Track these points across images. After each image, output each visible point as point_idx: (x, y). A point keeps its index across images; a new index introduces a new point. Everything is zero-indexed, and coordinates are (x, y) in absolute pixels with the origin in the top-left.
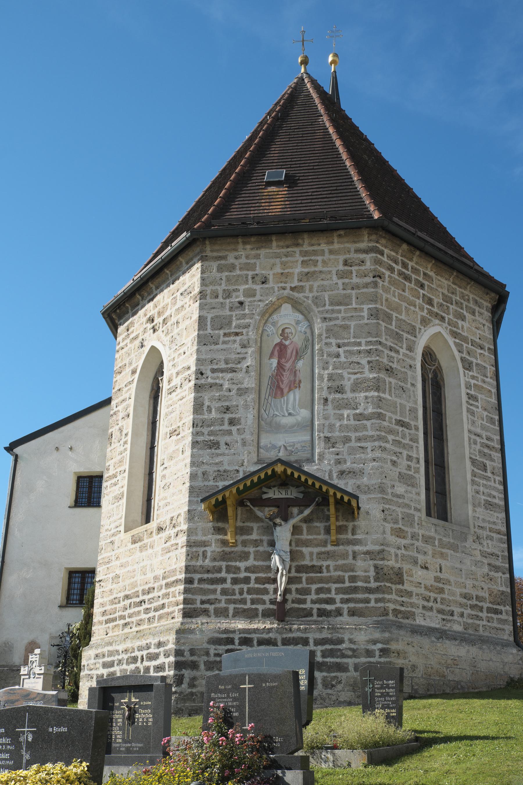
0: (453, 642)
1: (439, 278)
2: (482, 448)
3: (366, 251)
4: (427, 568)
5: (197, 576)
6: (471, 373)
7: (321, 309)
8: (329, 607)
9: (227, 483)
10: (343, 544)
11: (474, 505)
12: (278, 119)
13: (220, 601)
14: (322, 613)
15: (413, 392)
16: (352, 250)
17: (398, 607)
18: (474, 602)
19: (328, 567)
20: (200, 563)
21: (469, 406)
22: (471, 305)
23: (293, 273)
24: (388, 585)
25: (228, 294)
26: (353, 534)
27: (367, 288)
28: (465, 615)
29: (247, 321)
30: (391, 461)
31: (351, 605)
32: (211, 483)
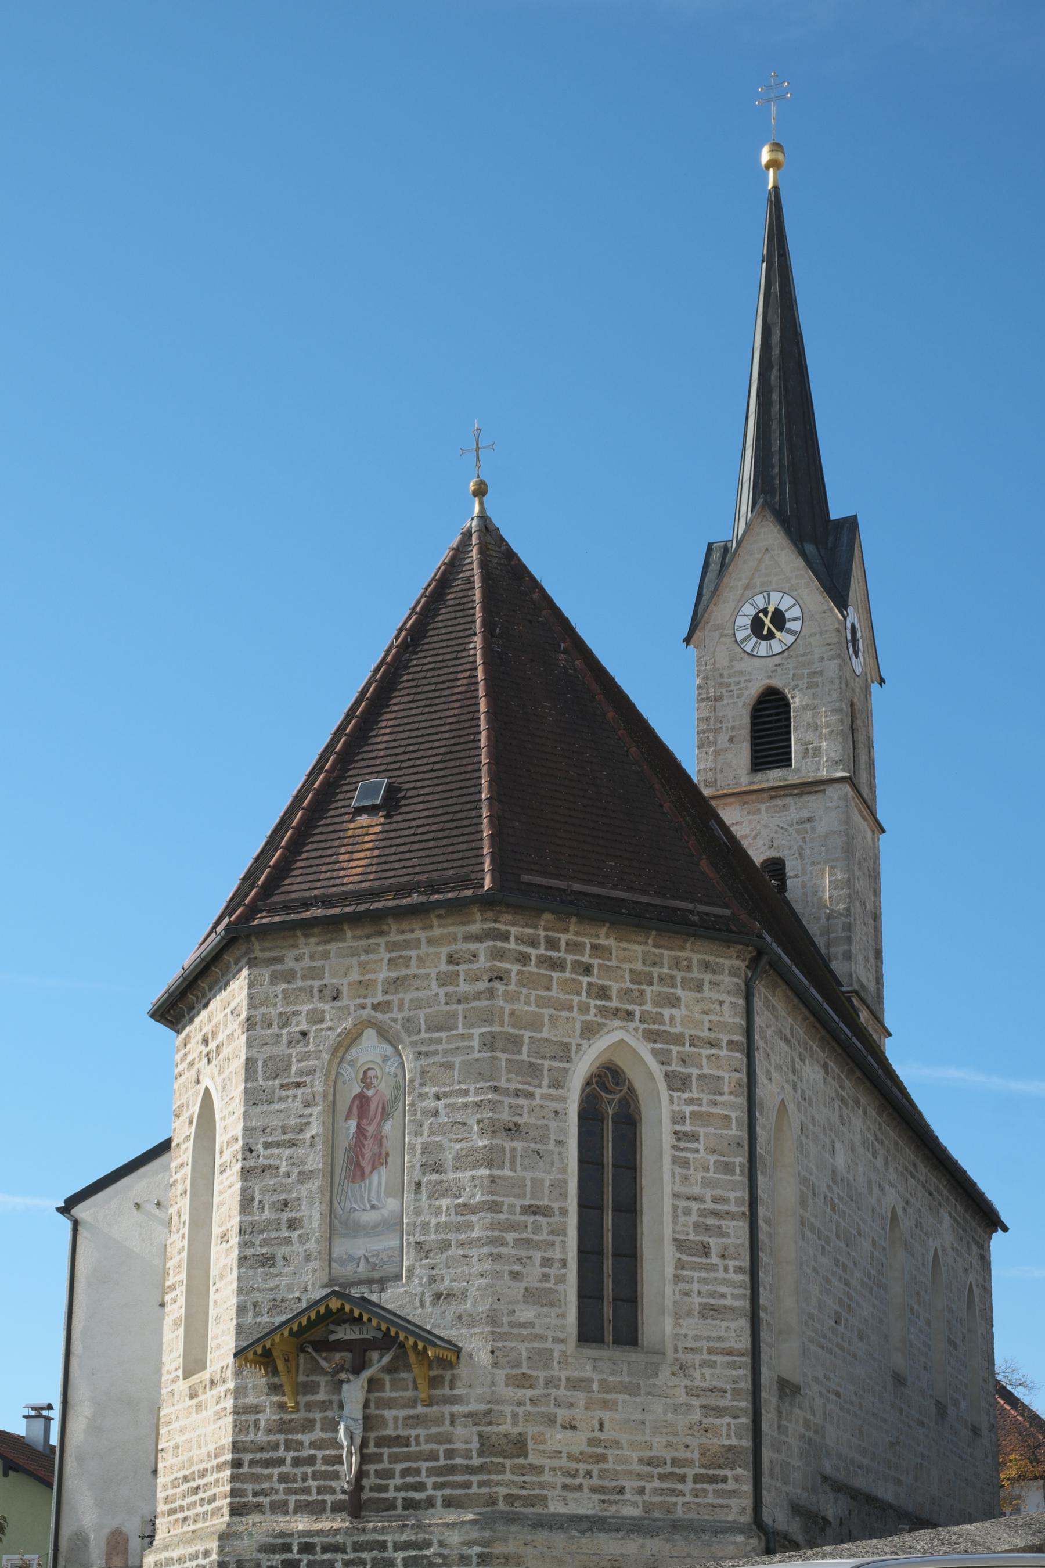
0: (614, 1535)
1: (625, 945)
2: (701, 1219)
3: (479, 938)
4: (573, 1428)
5: (247, 1457)
6: (686, 1096)
7: (414, 1038)
8: (418, 1496)
9: (284, 1318)
10: (437, 1404)
11: (677, 1316)
12: (407, 647)
13: (277, 1492)
14: (410, 1504)
15: (560, 1154)
16: (460, 936)
17: (515, 1491)
18: (669, 1469)
19: (417, 1437)
20: (251, 1437)
21: (677, 1153)
22: (696, 974)
23: (376, 981)
24: (496, 1460)
25: (285, 1020)
26: (451, 1389)
27: (479, 999)
28: (647, 1491)
29: (312, 1063)
30: (511, 1272)
31: (447, 1492)
32: (265, 1319)
